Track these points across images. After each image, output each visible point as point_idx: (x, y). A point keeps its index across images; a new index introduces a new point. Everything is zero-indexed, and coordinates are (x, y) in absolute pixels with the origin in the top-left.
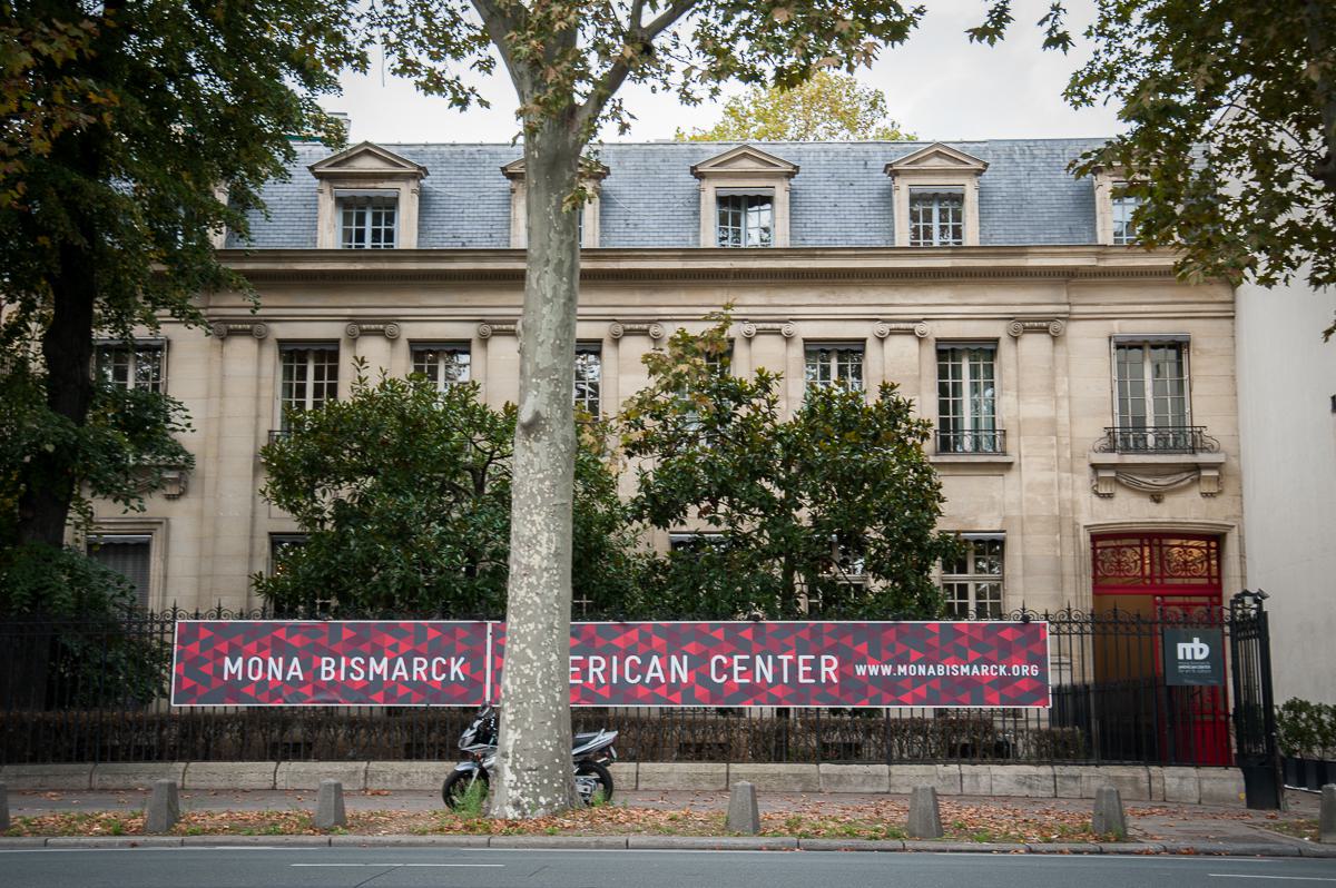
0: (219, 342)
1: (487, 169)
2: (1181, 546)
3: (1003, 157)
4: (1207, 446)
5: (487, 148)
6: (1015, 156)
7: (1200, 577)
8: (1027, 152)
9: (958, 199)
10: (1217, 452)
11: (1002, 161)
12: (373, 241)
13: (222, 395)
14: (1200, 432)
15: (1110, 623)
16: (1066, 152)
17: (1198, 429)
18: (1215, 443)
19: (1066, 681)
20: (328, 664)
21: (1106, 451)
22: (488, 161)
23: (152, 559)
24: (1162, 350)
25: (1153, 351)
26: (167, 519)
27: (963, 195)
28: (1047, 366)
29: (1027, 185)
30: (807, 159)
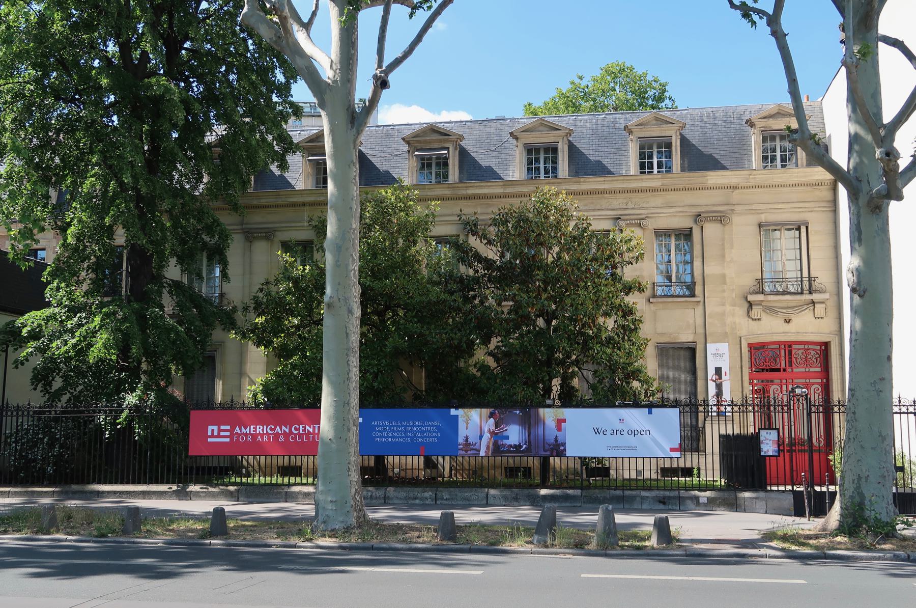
0: (249, 244)
1: (396, 139)
2: (804, 349)
3: (697, 118)
4: (818, 289)
5: (396, 127)
6: (704, 118)
7: (816, 367)
8: (711, 115)
9: (555, 150)
10: (825, 292)
11: (696, 120)
12: (776, 155)
13: (251, 273)
14: (814, 281)
15: (729, 405)
16: (735, 113)
17: (813, 279)
18: (823, 287)
19: (730, 432)
20: (260, 428)
21: (757, 293)
22: (396, 134)
23: (217, 364)
24: (793, 231)
25: (786, 232)
26: (223, 342)
27: (557, 148)
28: (721, 243)
29: (711, 135)
30: (579, 124)
